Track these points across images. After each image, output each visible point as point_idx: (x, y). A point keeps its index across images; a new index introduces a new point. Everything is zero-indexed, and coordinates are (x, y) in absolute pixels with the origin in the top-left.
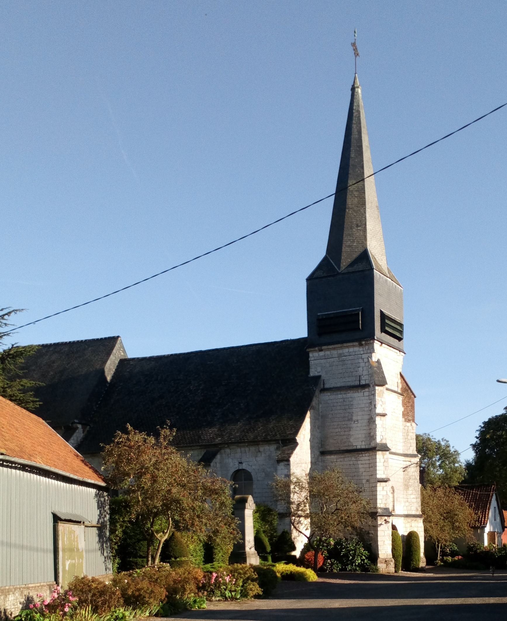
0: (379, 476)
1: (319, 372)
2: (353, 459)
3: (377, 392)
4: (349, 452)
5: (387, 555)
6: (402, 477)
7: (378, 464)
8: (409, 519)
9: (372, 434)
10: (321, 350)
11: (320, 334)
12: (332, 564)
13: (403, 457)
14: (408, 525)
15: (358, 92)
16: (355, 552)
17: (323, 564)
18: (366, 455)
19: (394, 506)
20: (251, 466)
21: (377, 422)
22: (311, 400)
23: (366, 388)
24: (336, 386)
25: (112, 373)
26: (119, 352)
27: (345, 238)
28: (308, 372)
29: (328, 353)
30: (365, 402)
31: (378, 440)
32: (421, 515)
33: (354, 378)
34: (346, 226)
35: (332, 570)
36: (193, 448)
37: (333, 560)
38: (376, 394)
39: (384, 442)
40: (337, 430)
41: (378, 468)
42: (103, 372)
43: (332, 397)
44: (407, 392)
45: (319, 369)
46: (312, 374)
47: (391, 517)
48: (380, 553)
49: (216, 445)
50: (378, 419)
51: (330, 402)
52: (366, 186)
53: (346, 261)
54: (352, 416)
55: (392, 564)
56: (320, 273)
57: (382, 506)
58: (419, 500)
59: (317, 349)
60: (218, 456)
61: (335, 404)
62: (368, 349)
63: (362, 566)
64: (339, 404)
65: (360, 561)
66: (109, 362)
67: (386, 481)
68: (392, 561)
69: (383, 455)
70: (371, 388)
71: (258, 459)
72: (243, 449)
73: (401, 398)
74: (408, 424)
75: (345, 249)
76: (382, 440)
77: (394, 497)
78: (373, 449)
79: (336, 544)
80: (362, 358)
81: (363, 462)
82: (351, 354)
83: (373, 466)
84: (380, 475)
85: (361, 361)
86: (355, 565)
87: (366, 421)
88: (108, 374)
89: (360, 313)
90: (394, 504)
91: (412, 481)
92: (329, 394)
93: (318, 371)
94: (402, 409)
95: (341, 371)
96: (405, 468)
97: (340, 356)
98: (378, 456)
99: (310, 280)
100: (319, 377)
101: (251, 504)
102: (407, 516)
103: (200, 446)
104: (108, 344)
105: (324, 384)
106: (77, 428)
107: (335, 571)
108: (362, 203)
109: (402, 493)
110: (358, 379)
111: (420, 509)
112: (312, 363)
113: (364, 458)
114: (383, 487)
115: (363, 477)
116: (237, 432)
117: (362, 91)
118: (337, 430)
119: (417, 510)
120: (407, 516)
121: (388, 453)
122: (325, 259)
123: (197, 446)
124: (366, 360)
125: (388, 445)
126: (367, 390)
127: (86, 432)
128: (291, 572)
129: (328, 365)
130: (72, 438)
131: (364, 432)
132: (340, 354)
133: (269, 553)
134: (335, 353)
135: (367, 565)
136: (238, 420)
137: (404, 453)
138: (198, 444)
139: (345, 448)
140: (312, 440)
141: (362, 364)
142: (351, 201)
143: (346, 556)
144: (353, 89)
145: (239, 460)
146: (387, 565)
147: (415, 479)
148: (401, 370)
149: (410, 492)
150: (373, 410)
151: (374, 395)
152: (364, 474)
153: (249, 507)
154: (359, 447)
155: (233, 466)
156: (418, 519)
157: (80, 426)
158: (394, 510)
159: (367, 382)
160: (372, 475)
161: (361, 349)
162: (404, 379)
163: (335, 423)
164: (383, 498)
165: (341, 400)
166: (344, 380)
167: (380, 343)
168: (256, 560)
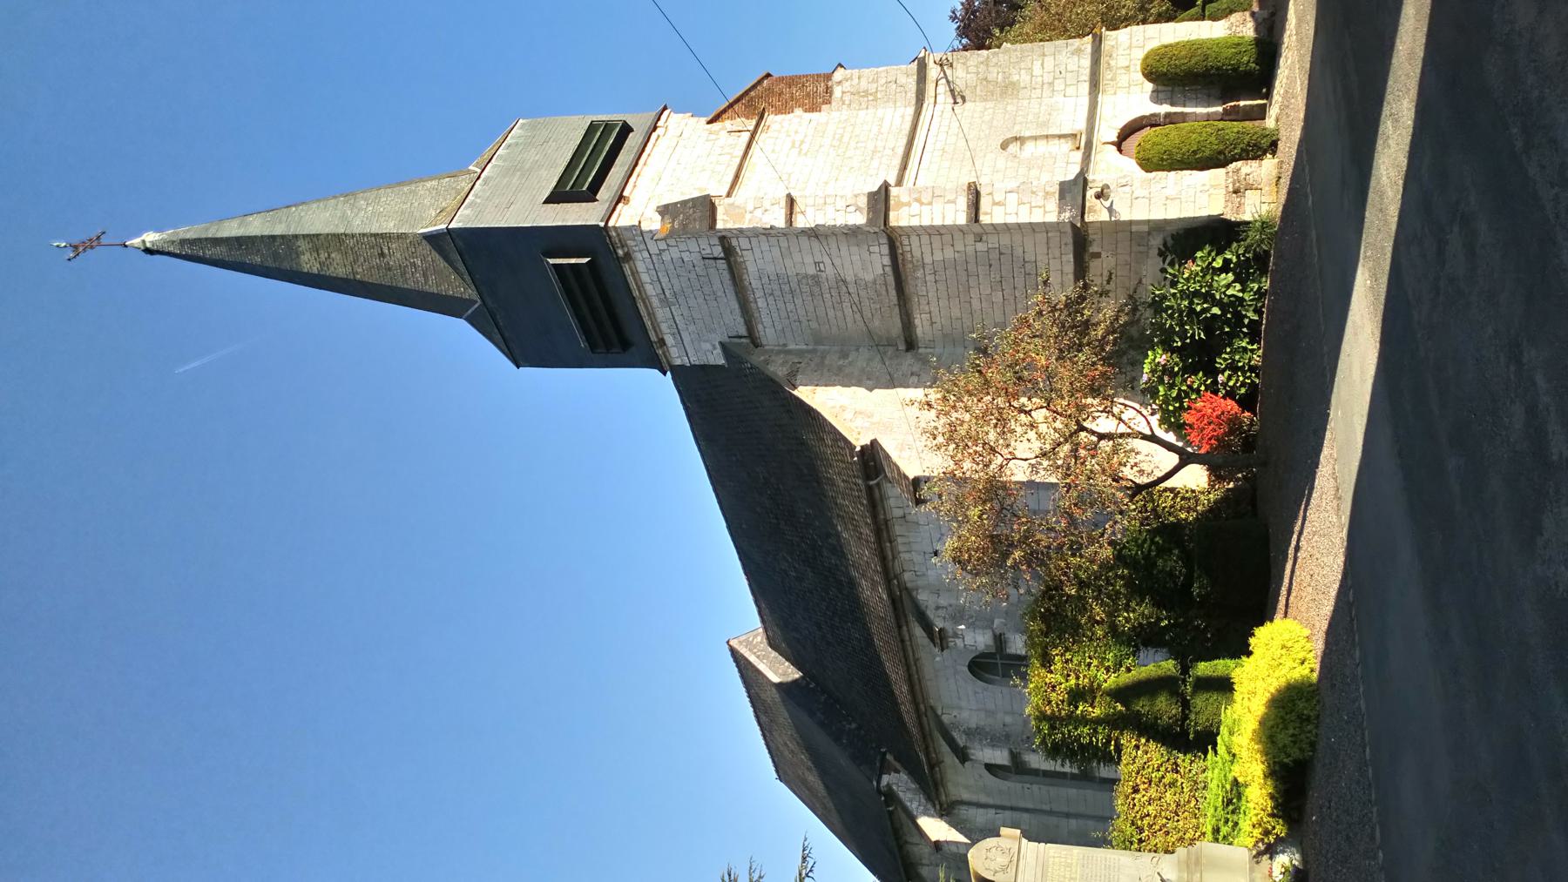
0: (958, 215)
2: (919, 274)
3: (729, 226)
4: (898, 296)
6: (979, 106)
8: (1106, 76)
10: (662, 342)
11: (625, 345)
12: (1233, 367)
14: (1123, 79)
16: (1196, 294)
17: (1230, 394)
19: (1060, 137)
24: (737, 311)
29: (664, 327)
30: (765, 246)
31: (860, 219)
32: (1095, 36)
33: (712, 271)
35: (1252, 369)
37: (1220, 363)
39: (863, 202)
40: (848, 311)
43: (766, 320)
44: (755, 101)
45: (708, 346)
47: (1090, 177)
48: (1204, 213)
50: (801, 222)
51: (779, 328)
54: (806, 276)
55: (1246, 168)
57: (1053, 205)
59: (660, 352)
60: (922, 596)
61: (784, 314)
64: (781, 305)
65: (1231, 277)
67: (978, 194)
73: (771, 119)
74: (837, 92)
76: (858, 209)
77: (1035, 138)
79: (1168, 347)
81: (927, 250)
84: (958, 215)
85: (666, 257)
89: (551, 261)
90: (1054, 136)
91: (994, 74)
92: (760, 327)
94: (798, 112)
95: (701, 300)
96: (957, 97)
97: (665, 301)
98: (903, 223)
99: (519, 358)
107: (1257, 359)
109: (1025, 102)
111: (1076, 42)
112: (695, 360)
113: (914, 249)
114: (995, 204)
115: (970, 249)
118: (848, 311)
119: (1078, 51)
121: (894, 191)
124: (663, 246)
126: (734, 242)
127: (898, 765)
129: (692, 328)
131: (844, 248)
132: (661, 301)
133: (1185, 670)
134: (661, 314)
137: (913, 101)
139: (893, 293)
141: (675, 253)
142: (339, 269)
143: (1210, 325)
144: (148, 251)
146: (1250, 187)
147: (986, 62)
149: (1024, 78)
151: (741, 231)
154: (887, 261)
156: (1107, 45)
157: (885, 779)
161: (638, 256)
162: (724, 111)
163: (831, 313)
164: (1024, 198)
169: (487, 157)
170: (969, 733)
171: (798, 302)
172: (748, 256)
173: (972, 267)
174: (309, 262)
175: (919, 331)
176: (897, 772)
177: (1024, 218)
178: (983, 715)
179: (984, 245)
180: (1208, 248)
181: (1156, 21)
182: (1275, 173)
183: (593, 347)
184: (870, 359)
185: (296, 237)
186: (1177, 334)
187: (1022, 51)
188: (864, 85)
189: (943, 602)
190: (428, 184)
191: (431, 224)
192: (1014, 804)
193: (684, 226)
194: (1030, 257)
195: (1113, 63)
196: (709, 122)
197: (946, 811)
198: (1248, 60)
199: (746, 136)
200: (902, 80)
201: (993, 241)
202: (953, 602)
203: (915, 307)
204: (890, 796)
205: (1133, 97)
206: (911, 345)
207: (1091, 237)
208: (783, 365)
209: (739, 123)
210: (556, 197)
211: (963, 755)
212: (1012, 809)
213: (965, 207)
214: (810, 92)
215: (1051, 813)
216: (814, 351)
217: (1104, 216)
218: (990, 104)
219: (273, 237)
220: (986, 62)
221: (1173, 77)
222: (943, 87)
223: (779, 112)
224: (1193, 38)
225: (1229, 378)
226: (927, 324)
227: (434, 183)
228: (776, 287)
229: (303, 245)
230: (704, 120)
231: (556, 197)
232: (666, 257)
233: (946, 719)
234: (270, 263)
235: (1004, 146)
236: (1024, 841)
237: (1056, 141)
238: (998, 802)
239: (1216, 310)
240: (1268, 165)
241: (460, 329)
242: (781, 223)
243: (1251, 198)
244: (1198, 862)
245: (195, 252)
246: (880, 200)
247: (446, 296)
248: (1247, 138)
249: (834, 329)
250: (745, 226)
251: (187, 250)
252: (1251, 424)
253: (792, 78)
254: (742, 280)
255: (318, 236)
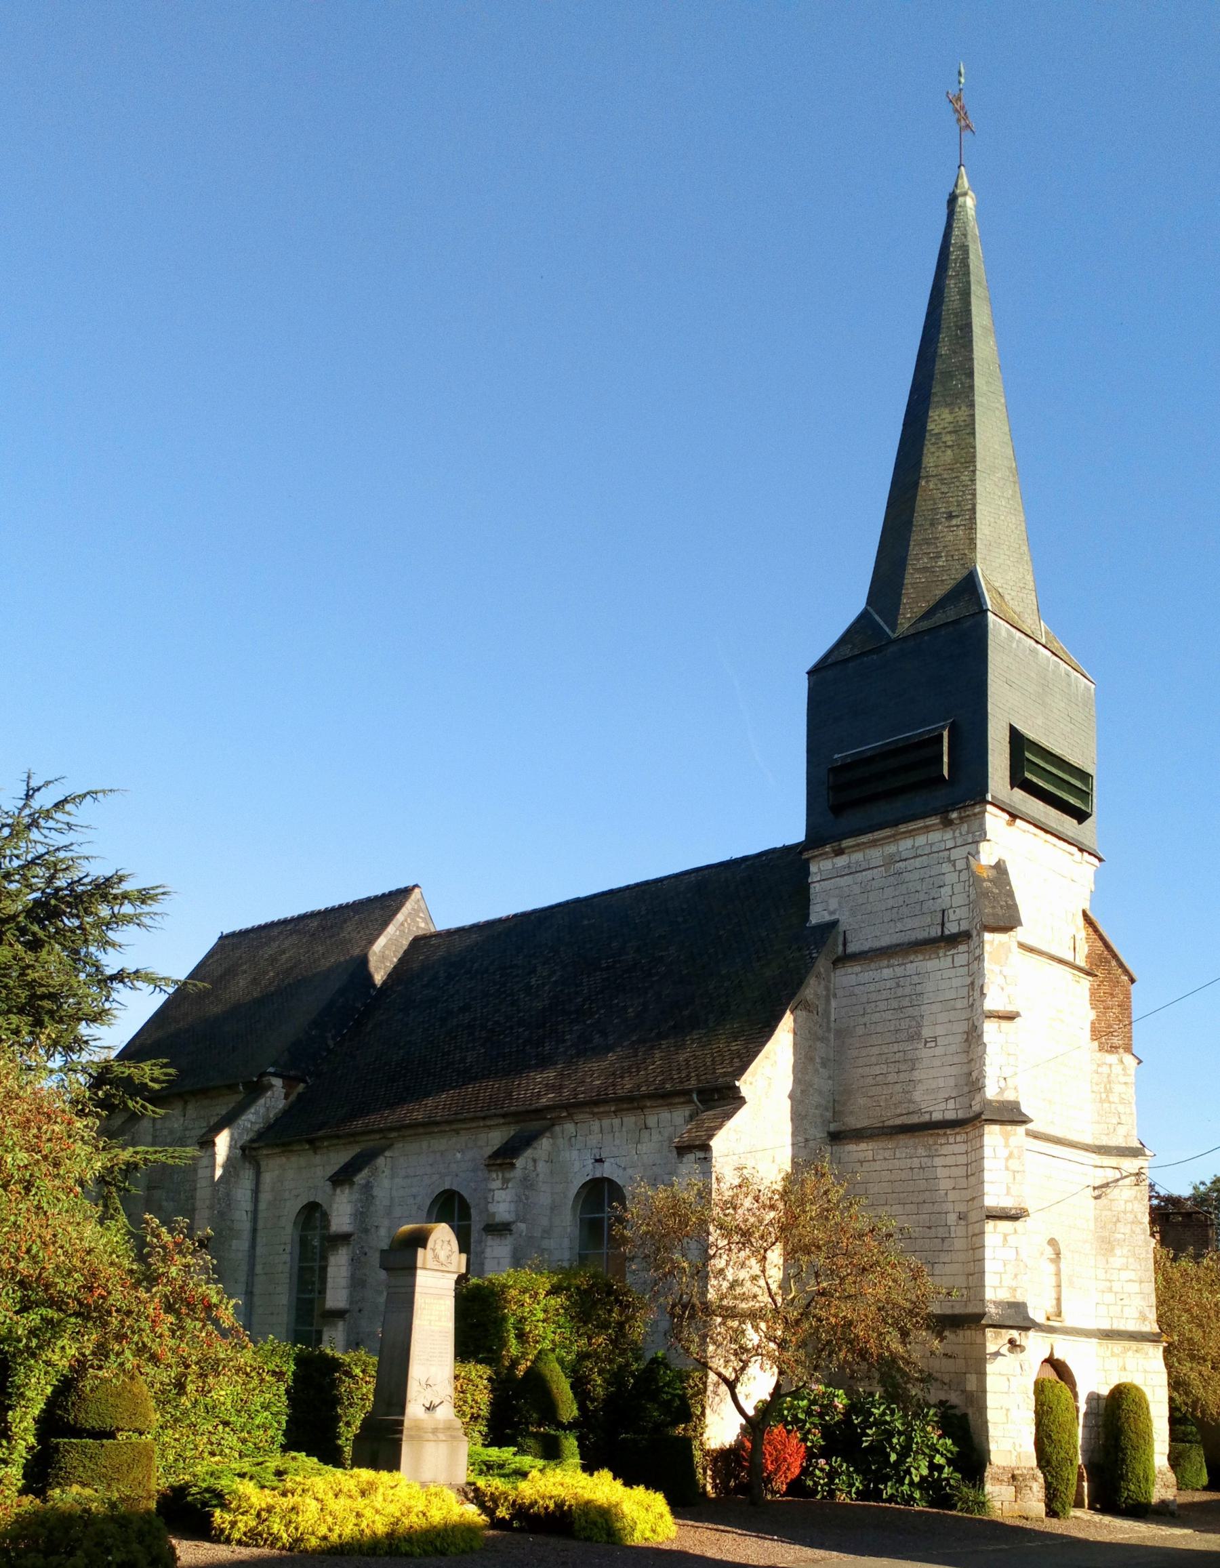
0: (993, 1198)
1: (832, 913)
2: (921, 1151)
3: (987, 947)
4: (905, 1129)
5: (1019, 1456)
7: (987, 1164)
8: (1118, 1346)
9: (974, 1075)
10: (839, 852)
11: (837, 809)
12: (832, 1475)
13: (1093, 1155)
15: (964, 206)
16: (910, 1439)
17: (805, 1471)
18: (959, 1139)
19: (1059, 1300)
20: (625, 1169)
21: (986, 1039)
22: (800, 983)
23: (960, 943)
25: (390, 965)
26: (413, 920)
27: (914, 550)
28: (807, 917)
29: (858, 856)
30: (956, 982)
32: (1159, 1335)
34: (918, 519)
35: (832, 1493)
36: (489, 1123)
37: (836, 1461)
38: (986, 955)
39: (1009, 1096)
40: (877, 1070)
41: (987, 1176)
42: (363, 961)
43: (866, 976)
44: (1106, 966)
45: (833, 904)
46: (814, 920)
47: (1031, 1333)
48: (993, 1447)
49: (539, 1113)
50: (990, 1029)
51: (857, 990)
52: (977, 417)
53: (912, 608)
54: (920, 1026)
56: (847, 651)
57: (1004, 1295)
58: (1150, 1288)
59: (828, 849)
60: (545, 1143)
61: (874, 997)
62: (968, 833)
63: (933, 1488)
64: (885, 994)
65: (925, 1472)
66: (381, 941)
67: (1014, 1218)
68: (1035, 1478)
69: (1006, 1137)
70: (973, 944)
71: (643, 1148)
72: (606, 1122)
73: (1086, 983)
74: (1112, 1058)
75: (912, 578)
76: (1002, 1090)
77: (1058, 1274)
78: (972, 1117)
79: (851, 1409)
80: (949, 860)
81: (950, 1160)
82: (919, 852)
83: (974, 1171)
84: (993, 1198)
85: (946, 867)
86: (912, 1483)
87: (960, 1038)
88: (377, 968)
89: (946, 734)
92: (857, 969)
93: (831, 908)
94: (1092, 1015)
95: (891, 903)
96: (1101, 1190)
97: (891, 861)
98: (988, 1140)
100: (835, 924)
101: (442, 1255)
102: (1109, 1335)
103: (504, 1116)
104: (386, 905)
105: (845, 945)
106: (271, 1086)
107: (842, 1497)
108: (968, 460)
110: (940, 921)
111: (1152, 1315)
112: (816, 888)
113: (952, 1147)
114: (1005, 1236)
115: (950, 1207)
116: (598, 1078)
117: (977, 207)
118: (877, 1070)
120: (1109, 1335)
121: (1021, 1130)
122: (864, 617)
123: (495, 1115)
124: (961, 865)
125: (1024, 1110)
126: (962, 948)
127: (292, 1097)
128: (559, 1505)
129: (857, 890)
130: (253, 1110)
131: (954, 1070)
132: (891, 856)
133: (570, 1427)
135: (948, 1484)
136: (610, 1049)
137: (1098, 1143)
138: (499, 1111)
139: (898, 1121)
140: (798, 1098)
141: (951, 878)
142: (933, 459)
143: (878, 1450)
144: (953, 200)
145: (596, 1151)
147: (1136, 1222)
148: (1086, 906)
149: (1117, 1261)
150: (977, 1004)
151: (980, 958)
152: (952, 1196)
153: (431, 1263)
154: (937, 1116)
155: (581, 1170)
157: (277, 1082)
158: (1059, 1314)
159: (964, 926)
160: (974, 1199)
161: (948, 835)
162: (1096, 930)
163: (875, 1050)
164: (1009, 1268)
165: (889, 984)
166: (899, 926)
167: (1007, 817)
168: (453, 1453)
169: (1055, 646)
170: (368, 1187)
171: (888, 1015)
172: (946, 962)
173: (927, 1208)
174: (939, 419)
175: (852, 1147)
176: (286, 1097)
177: (989, 1266)
178: (386, 1202)
179: (964, 1222)
180: (955, 1449)
181: (1171, 1399)
182: (1032, 1514)
183: (835, 771)
184: (820, 1092)
185: (972, 405)
186: (865, 1420)
187: (1146, 1259)
188: (1118, 1088)
189: (541, 1166)
190: (1030, 578)
191: (987, 583)
192: (260, 1234)
193: (985, 894)
194: (938, 1269)
195: (1130, 1353)
196: (1085, 914)
197: (245, 1153)
198: (1131, 1488)
199: (1070, 958)
200: (1122, 1130)
201: (959, 1231)
202: (541, 1177)
203: (881, 1145)
204: (256, 1090)
205: (1096, 1374)
206: (836, 1137)
207: (961, 1333)
208: (816, 994)
209: (1083, 949)
210: (1017, 740)
211: (342, 1178)
212: (254, 1231)
213: (1002, 1205)
214: (1114, 1029)
215: (251, 1273)
216: (829, 1030)
217: (991, 1348)
218: (1092, 1225)
219: (971, 374)
220: (1136, 1222)
221: (1115, 1414)
222: (1113, 1175)
223: (1093, 993)
224: (1155, 1436)
225: (822, 1470)
226: (861, 1156)
227: (1031, 585)
228: (907, 991)
229: (962, 413)
230: (1087, 906)
231: (1017, 740)
232: (946, 867)
233: (381, 1161)
234: (939, 366)
235: (1052, 1242)
236: (455, 1276)
237: (1054, 1295)
238: (261, 1215)
239: (893, 1457)
240: (1039, 1508)
241: (850, 601)
242: (989, 1004)
243: (1007, 1492)
244: (453, 1438)
245: (949, 264)
246: (1011, 1115)
247: (900, 595)
248: (1062, 1488)
249: (855, 1053)
250: (986, 965)
251: (955, 254)
252: (774, 1492)
253: (1129, 1008)
254: (916, 952)
255: (973, 434)
